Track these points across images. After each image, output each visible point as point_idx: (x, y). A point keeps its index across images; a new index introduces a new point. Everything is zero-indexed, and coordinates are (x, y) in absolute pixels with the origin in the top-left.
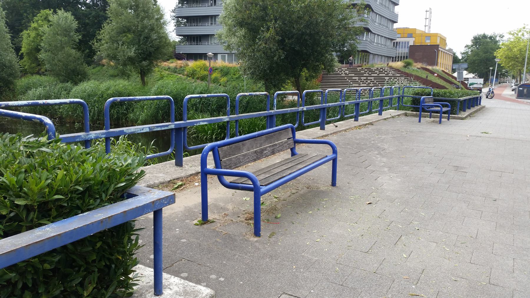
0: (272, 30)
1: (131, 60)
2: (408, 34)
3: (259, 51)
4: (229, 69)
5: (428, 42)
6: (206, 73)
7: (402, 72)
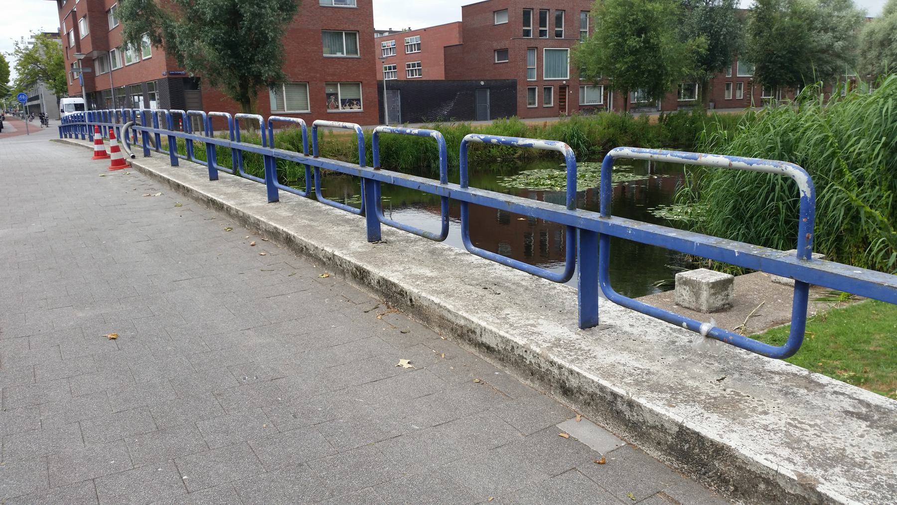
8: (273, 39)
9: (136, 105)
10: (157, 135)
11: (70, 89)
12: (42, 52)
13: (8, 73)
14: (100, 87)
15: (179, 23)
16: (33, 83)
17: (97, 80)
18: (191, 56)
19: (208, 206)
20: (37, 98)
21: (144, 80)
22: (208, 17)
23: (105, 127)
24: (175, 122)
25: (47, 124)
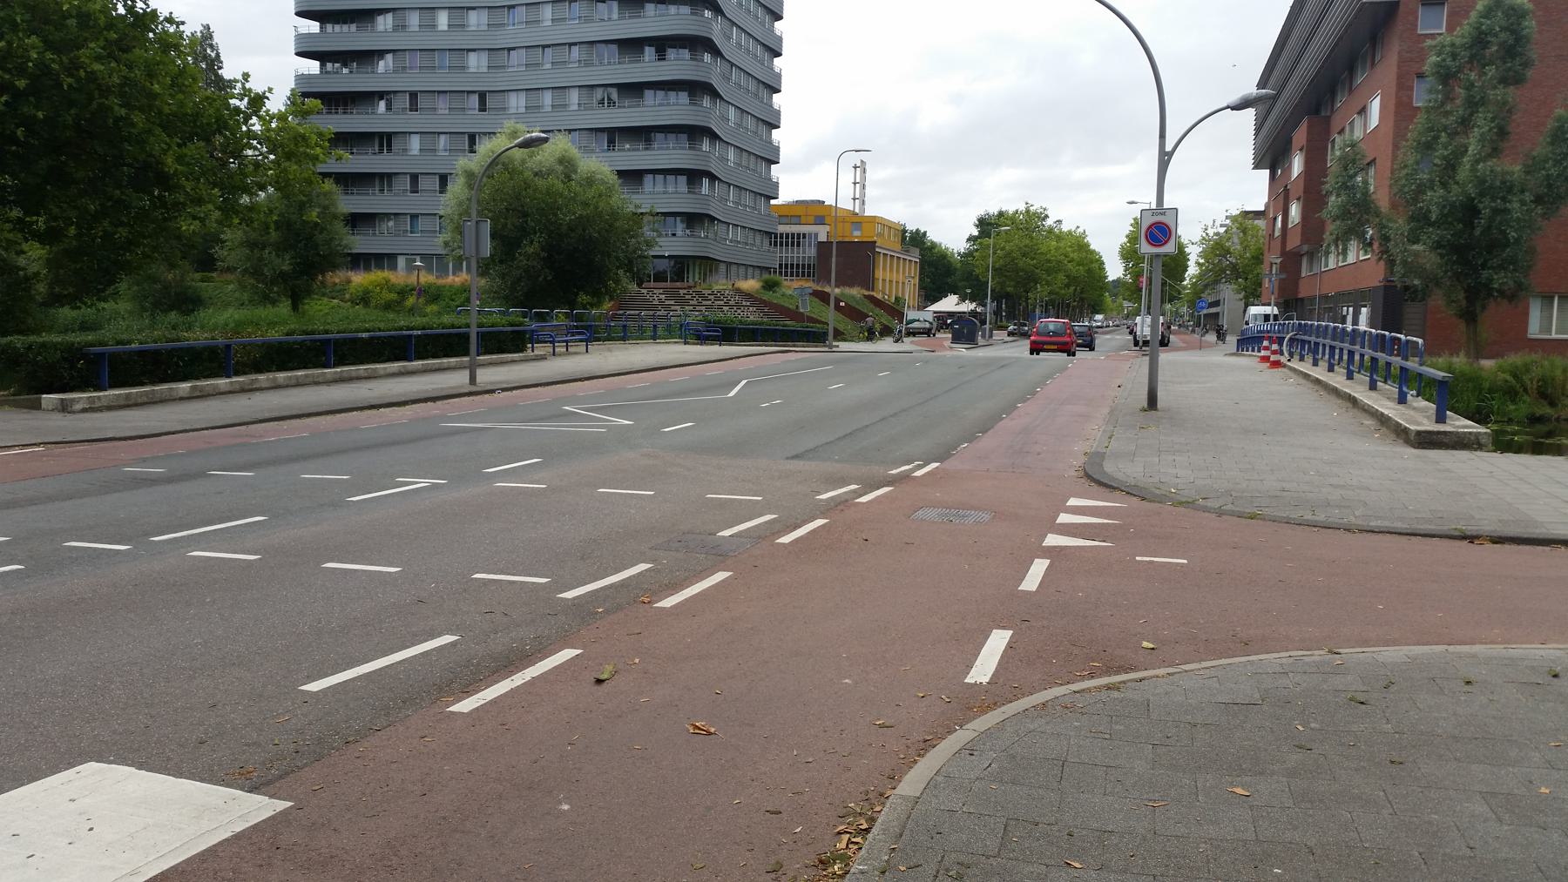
0: (536, 245)
1: (283, 276)
2: (817, 217)
4: (439, 288)
5: (857, 236)
6: (393, 296)
7: (756, 299)
8: (1517, 241)
9: (1344, 321)
11: (1264, 292)
12: (1236, 240)
14: (1303, 293)
15: (1400, 225)
16: (1217, 282)
17: (1301, 283)
18: (1404, 263)
19: (1398, 435)
22: (1434, 217)
23: (1341, 350)
24: (1380, 344)
25: (1223, 340)
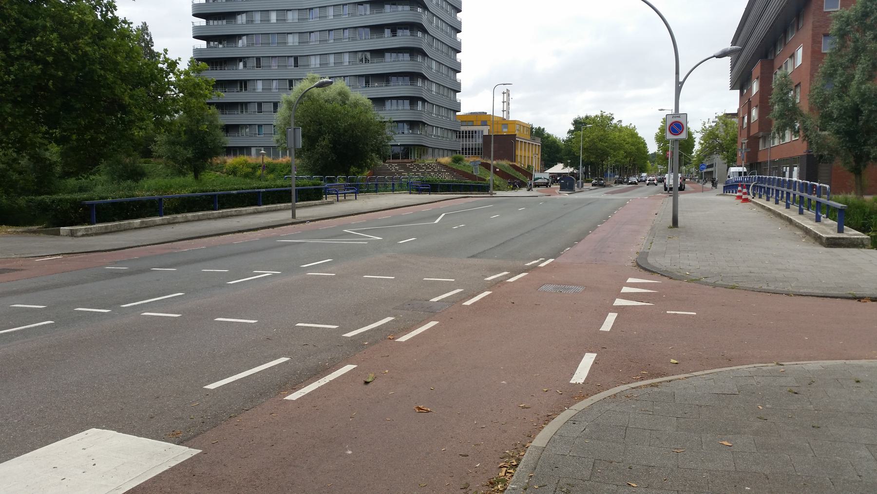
3: (317, 153)
4: (275, 165)
5: (505, 131)
6: (250, 170)
10: (794, 195)
12: (721, 130)
13: (693, 146)
14: (761, 159)
15: (814, 120)
16: (711, 153)
17: (760, 154)
20: (711, 166)
21: (792, 155)
